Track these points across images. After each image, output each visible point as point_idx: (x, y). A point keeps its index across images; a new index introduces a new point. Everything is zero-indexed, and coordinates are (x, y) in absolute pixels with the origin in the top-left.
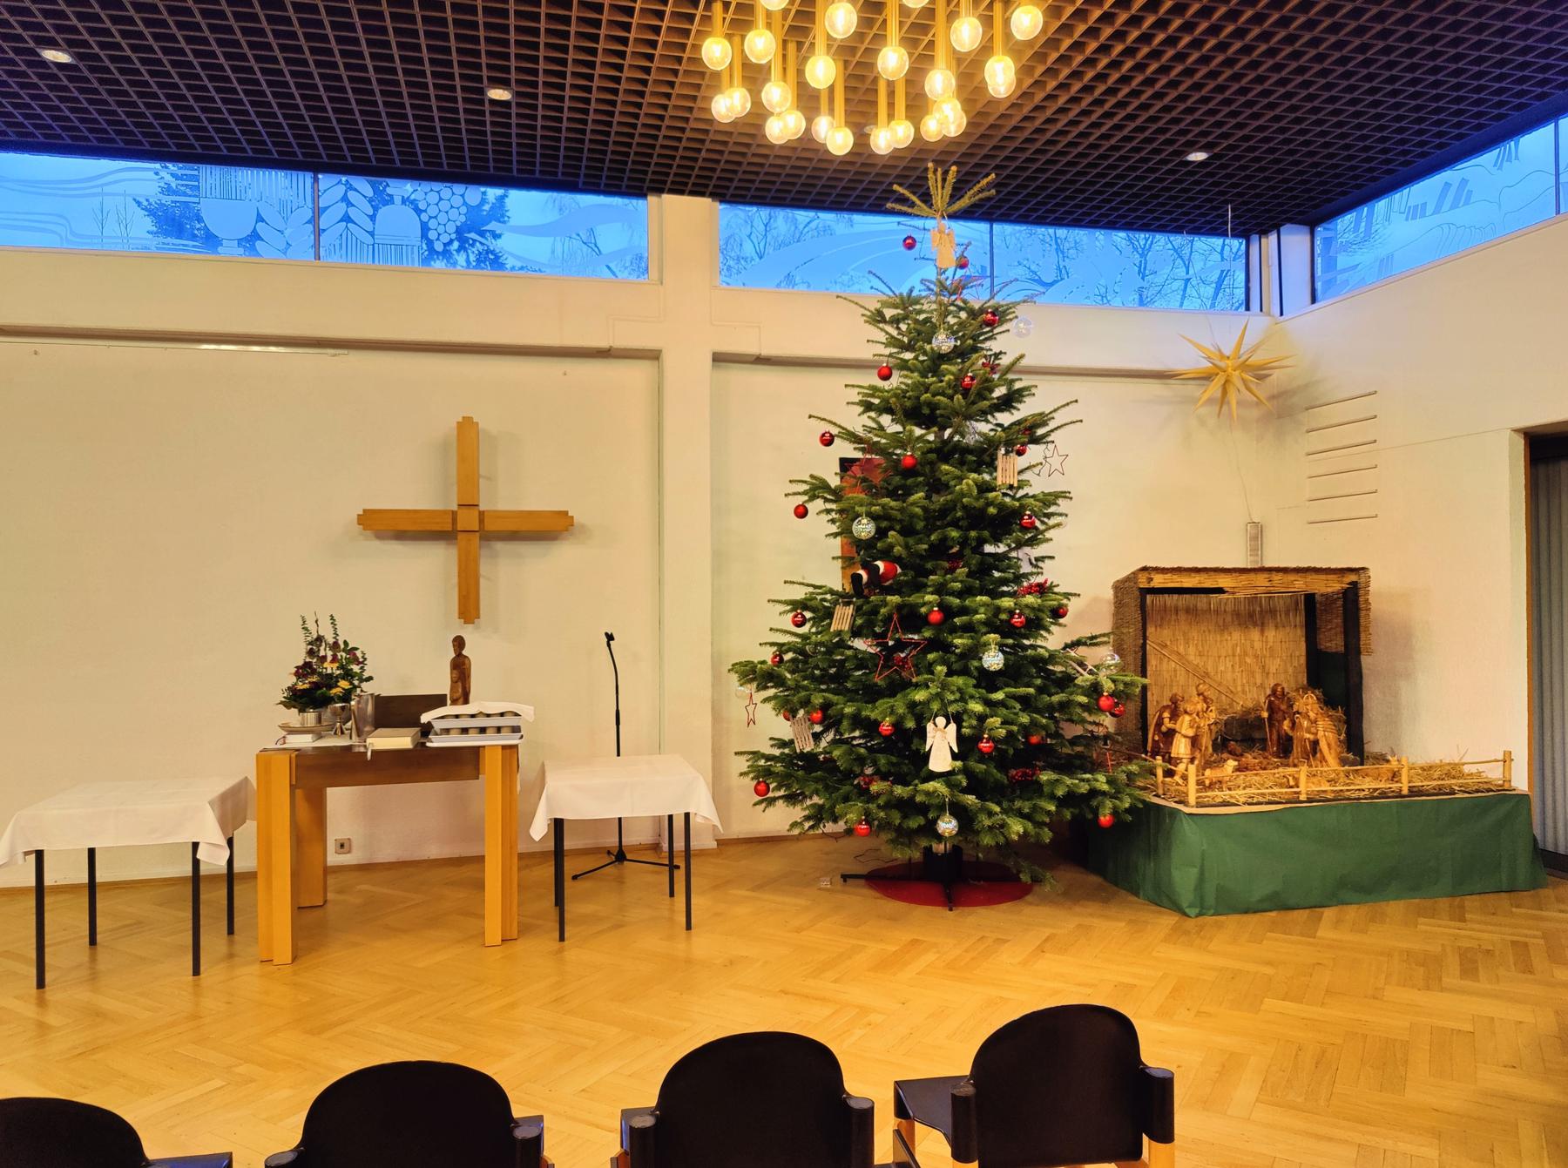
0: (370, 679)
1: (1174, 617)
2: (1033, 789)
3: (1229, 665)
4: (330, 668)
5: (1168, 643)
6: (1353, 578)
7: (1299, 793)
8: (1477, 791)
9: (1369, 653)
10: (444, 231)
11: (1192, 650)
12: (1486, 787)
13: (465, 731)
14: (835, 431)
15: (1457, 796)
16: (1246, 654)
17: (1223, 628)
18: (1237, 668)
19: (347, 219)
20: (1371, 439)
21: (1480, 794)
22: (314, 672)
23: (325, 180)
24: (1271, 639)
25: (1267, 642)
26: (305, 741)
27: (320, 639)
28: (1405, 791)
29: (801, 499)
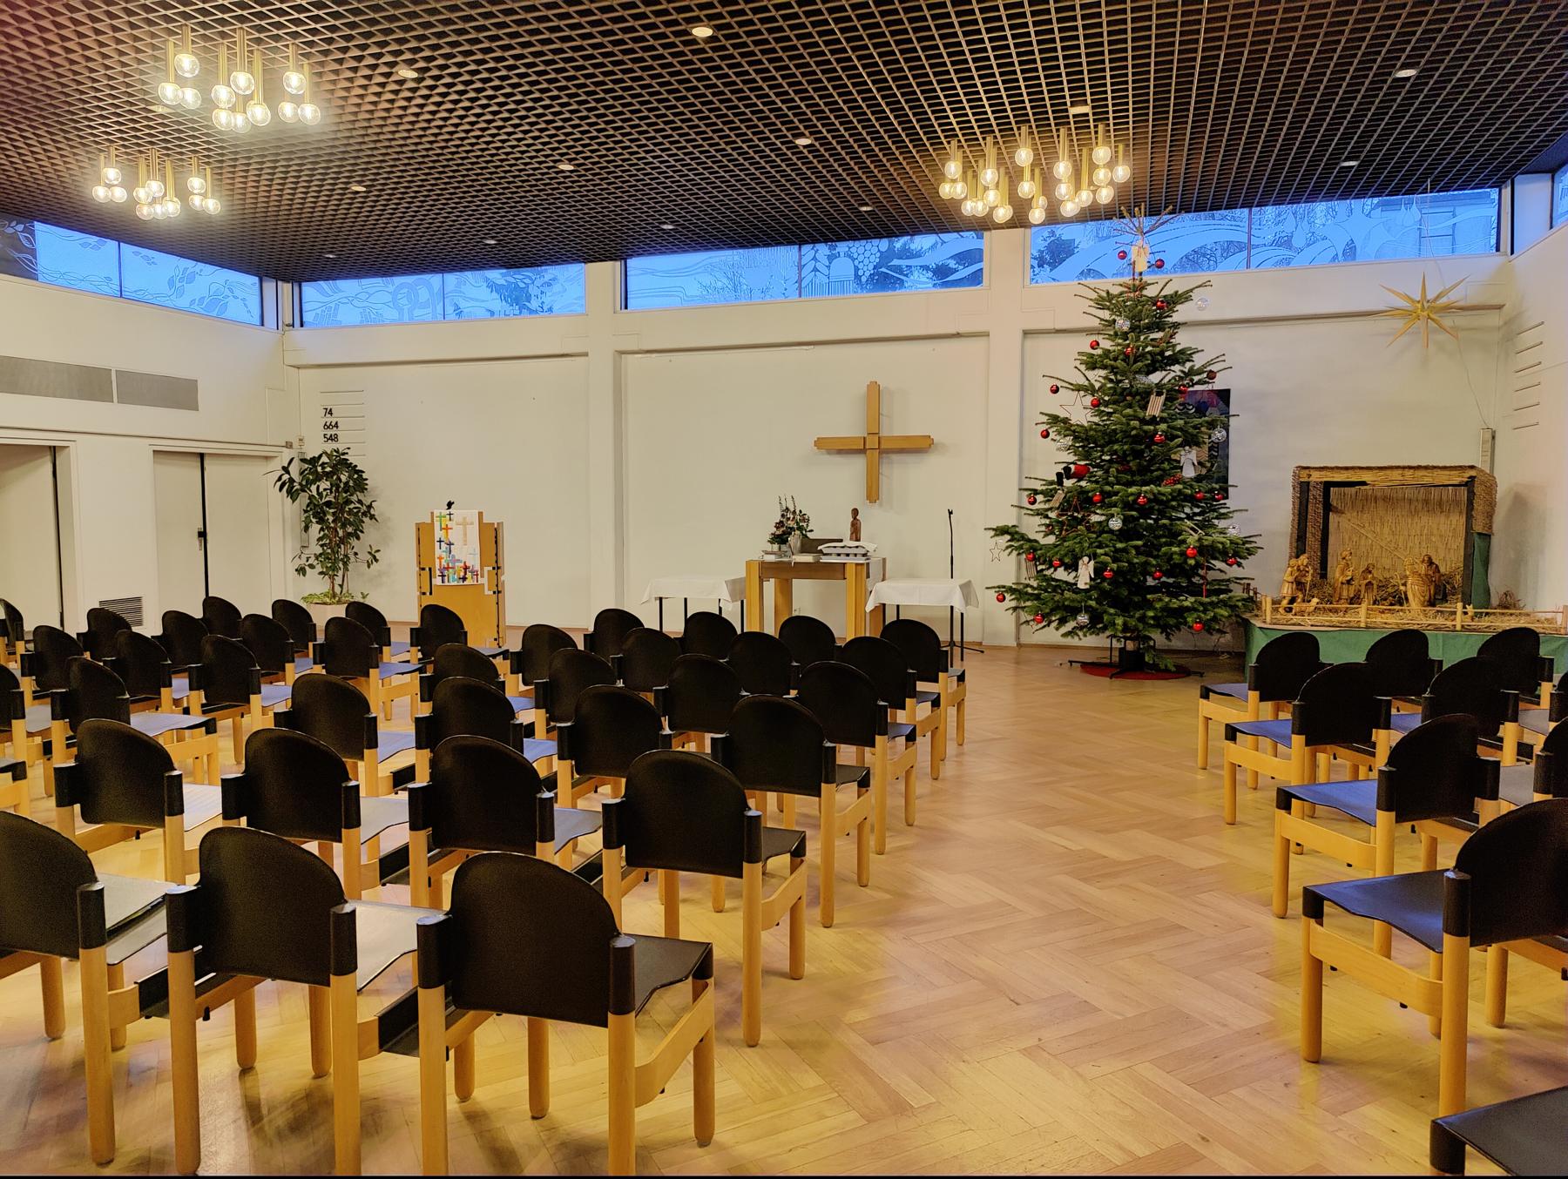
0: (811, 531)
2: (1149, 605)
3: (1417, 542)
4: (791, 524)
5: (1367, 525)
6: (1473, 473)
10: (867, 271)
11: (1386, 530)
13: (839, 555)
14: (1059, 384)
16: (1432, 534)
17: (1414, 513)
19: (815, 270)
20: (1537, 361)
22: (783, 526)
23: (806, 248)
24: (1454, 522)
26: (772, 558)
27: (787, 509)
29: (1045, 427)
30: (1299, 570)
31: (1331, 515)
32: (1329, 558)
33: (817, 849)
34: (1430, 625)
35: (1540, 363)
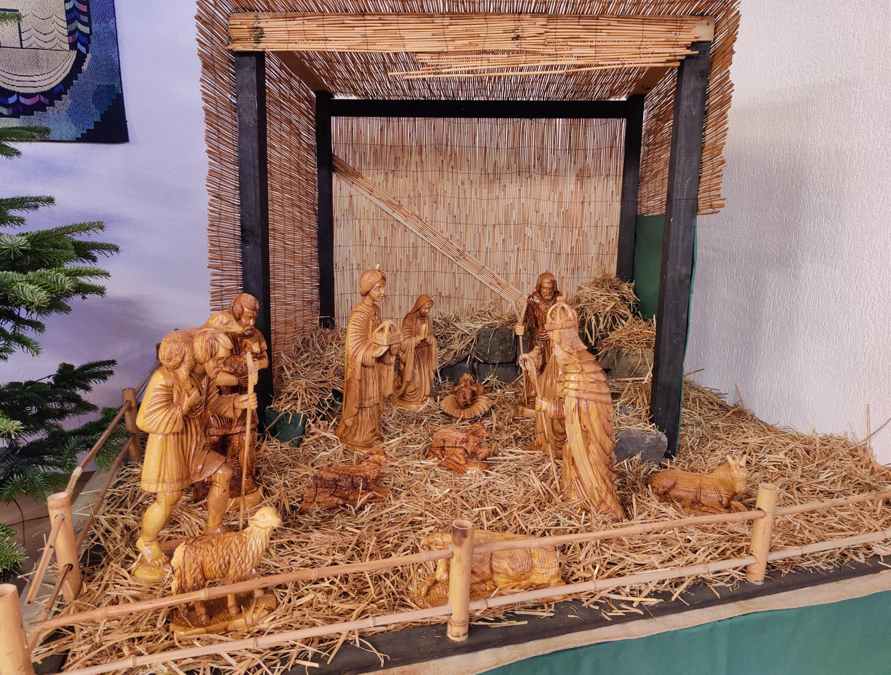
1: (415, 158)
3: (499, 239)
5: (405, 201)
9: (714, 209)
11: (442, 214)
16: (526, 222)
18: (511, 244)
25: (560, 202)
28: (757, 576)
31: (340, 186)
32: (337, 275)
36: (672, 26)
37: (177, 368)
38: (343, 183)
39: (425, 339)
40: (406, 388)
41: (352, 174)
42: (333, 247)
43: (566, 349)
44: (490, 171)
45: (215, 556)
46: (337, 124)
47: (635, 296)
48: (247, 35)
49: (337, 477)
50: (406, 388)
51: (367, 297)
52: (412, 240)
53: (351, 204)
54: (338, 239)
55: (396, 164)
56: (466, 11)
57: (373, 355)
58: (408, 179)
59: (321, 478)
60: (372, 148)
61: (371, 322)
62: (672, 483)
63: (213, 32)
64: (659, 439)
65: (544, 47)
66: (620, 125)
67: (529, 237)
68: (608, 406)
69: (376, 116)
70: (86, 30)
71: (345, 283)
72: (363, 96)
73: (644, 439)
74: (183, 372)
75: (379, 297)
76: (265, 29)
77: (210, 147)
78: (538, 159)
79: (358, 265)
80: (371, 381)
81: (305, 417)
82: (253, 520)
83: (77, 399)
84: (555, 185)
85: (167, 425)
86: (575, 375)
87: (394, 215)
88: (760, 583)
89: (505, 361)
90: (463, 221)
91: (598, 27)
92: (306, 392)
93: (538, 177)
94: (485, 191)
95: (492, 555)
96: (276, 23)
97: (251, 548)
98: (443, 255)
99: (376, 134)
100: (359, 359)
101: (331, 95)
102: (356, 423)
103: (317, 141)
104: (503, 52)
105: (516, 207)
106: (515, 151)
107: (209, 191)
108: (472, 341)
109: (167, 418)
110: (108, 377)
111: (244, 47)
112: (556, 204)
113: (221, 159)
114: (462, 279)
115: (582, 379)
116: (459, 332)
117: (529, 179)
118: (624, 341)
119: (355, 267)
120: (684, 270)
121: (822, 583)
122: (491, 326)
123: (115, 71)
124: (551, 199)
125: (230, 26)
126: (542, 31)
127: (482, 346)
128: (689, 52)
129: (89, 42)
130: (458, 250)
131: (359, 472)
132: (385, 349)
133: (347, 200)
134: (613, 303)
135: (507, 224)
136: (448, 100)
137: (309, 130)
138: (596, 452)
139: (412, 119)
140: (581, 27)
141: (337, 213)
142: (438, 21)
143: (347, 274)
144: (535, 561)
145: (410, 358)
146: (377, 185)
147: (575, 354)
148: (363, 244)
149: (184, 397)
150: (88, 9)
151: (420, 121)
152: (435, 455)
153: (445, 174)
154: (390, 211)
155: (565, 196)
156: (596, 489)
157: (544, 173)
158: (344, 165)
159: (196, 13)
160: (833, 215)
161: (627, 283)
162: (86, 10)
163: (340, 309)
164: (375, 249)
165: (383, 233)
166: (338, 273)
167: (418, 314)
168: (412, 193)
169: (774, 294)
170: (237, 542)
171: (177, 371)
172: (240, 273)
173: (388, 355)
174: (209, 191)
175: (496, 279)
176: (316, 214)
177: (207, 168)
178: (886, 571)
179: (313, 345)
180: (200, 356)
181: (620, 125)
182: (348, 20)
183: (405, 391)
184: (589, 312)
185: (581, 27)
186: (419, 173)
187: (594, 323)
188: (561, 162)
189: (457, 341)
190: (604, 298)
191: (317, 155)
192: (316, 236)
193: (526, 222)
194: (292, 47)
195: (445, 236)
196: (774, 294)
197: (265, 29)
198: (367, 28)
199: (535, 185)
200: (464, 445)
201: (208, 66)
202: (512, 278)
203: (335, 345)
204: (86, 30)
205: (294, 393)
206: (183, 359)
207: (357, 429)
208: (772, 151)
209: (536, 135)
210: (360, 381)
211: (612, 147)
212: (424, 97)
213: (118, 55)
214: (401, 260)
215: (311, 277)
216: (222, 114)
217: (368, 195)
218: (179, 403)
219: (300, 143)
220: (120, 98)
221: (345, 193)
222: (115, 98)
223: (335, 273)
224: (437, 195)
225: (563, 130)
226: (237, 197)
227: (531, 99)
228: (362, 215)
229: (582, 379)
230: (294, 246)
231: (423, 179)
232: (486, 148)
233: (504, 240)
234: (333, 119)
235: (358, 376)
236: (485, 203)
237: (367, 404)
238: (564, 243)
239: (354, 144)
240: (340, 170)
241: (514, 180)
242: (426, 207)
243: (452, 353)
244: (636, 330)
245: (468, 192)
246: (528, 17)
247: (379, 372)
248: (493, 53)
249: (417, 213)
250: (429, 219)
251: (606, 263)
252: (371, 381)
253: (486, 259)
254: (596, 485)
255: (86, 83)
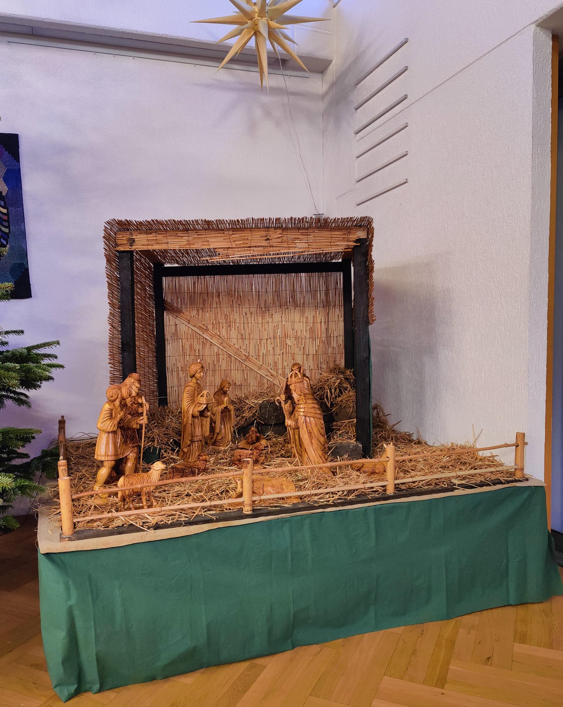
1: (215, 299)
5: (210, 327)
7: (242, 503)
8: (482, 485)
11: (234, 334)
12: (493, 477)
15: (456, 493)
16: (286, 336)
18: (278, 351)
21: (485, 489)
28: (390, 491)
30: (123, 405)
31: (169, 319)
32: (168, 375)
33: (239, 278)
34: (350, 492)
35: (405, 97)
36: (346, 232)
37: (114, 401)
38: (171, 317)
39: (227, 407)
40: (217, 437)
41: (176, 311)
42: (165, 357)
43: (298, 393)
44: (262, 306)
45: (138, 481)
46: (166, 281)
47: (354, 377)
48: (126, 242)
49: (184, 467)
50: (217, 437)
51: (194, 378)
52: (216, 351)
53: (176, 330)
54: (168, 352)
55: (204, 305)
56: (240, 227)
57: (198, 410)
58: (211, 313)
59: (176, 468)
60: (189, 294)
61: (196, 392)
62: (362, 465)
63: (110, 243)
64: (357, 446)
65: (281, 244)
66: (340, 276)
67: (289, 346)
68: (321, 420)
69: (191, 276)
70: (6, 230)
71: (174, 380)
72: (182, 264)
73: (349, 446)
74: (117, 403)
75: (200, 377)
76: (135, 239)
77: (110, 301)
78: (292, 297)
79: (182, 368)
80: (197, 426)
81: (160, 449)
82: (153, 466)
83: (16, 452)
84: (303, 312)
85: (111, 426)
86: (303, 405)
87: (204, 335)
88: (392, 494)
89: (278, 423)
90: (247, 337)
91: (308, 233)
92: (159, 437)
93: (292, 309)
94: (260, 318)
95: (263, 485)
96: (141, 236)
97: (152, 479)
98: (236, 359)
99: (191, 286)
100: (191, 412)
101: (163, 264)
102: (189, 451)
103: (154, 292)
104: (262, 246)
105: (280, 327)
106: (277, 293)
107: (109, 323)
108: (257, 411)
109: (111, 424)
110: (32, 441)
111: (124, 248)
112: (304, 324)
113: (114, 307)
114: (248, 374)
115: (306, 406)
116: (248, 406)
117: (287, 310)
118: (344, 400)
119: (180, 369)
120: (365, 355)
121: (425, 495)
122: (267, 401)
123: (24, 254)
124: (301, 321)
125: (116, 238)
126: (280, 236)
127: (264, 414)
128: (355, 244)
129: (8, 237)
130: (245, 355)
131: (195, 465)
132: (205, 406)
133: (173, 328)
134: (339, 381)
135: (275, 337)
136: (234, 265)
137: (150, 286)
138: (316, 443)
139: (212, 276)
140: (300, 233)
141: (168, 336)
142: (226, 232)
143: (175, 374)
144: (284, 487)
145: (218, 418)
146: (192, 317)
147: (303, 395)
148: (184, 355)
149: (117, 414)
150: (8, 218)
151: (217, 277)
152: (236, 464)
153: (235, 308)
154: (201, 333)
155: (309, 319)
156: (317, 462)
157: (296, 305)
158: (171, 306)
159: (103, 235)
160: (448, 323)
161: (349, 370)
162: (7, 219)
163: (171, 397)
164: (192, 357)
165: (197, 347)
166: (169, 374)
167: (222, 391)
168: (214, 321)
169: (429, 370)
170: (146, 476)
171: (114, 403)
172: (121, 368)
173: (206, 411)
174: (109, 323)
175: (270, 372)
176: (154, 337)
177: (109, 311)
178: (457, 490)
179: (157, 416)
180: (125, 395)
181: (340, 276)
182: (180, 234)
183: (216, 439)
184: (326, 387)
185: (300, 233)
186: (219, 309)
187: (329, 394)
188: (306, 299)
189: (247, 411)
190: (334, 379)
191: (155, 300)
192: (154, 350)
193: (286, 336)
194: (150, 248)
195: (236, 347)
196: (429, 370)
197: (135, 239)
198: (189, 237)
199: (290, 313)
200: (251, 456)
201: (109, 261)
202: (280, 371)
203: (170, 416)
204: (6, 230)
205: (152, 437)
206: (118, 396)
207: (190, 454)
208: (420, 289)
209: (290, 284)
210: (191, 424)
211: (336, 289)
212: (220, 263)
213: (26, 245)
214: (209, 363)
215: (153, 375)
216: (114, 283)
217: (187, 324)
218: (116, 417)
219: (146, 294)
220: (27, 270)
221: (172, 323)
222: (23, 270)
223: (167, 374)
224: (230, 322)
225: (306, 280)
226: (120, 326)
227: (285, 262)
228: (183, 336)
229: (306, 406)
230: (144, 355)
231: (221, 313)
232: (259, 292)
233: (273, 348)
234: (164, 278)
235: (190, 422)
236: (260, 325)
237: (195, 439)
238: (311, 347)
239: (177, 292)
240: (169, 309)
241: (277, 311)
242: (224, 329)
243: (244, 419)
244: (351, 394)
245: (249, 319)
246: (272, 229)
247: (201, 422)
248: (256, 247)
249: (218, 333)
250: (226, 337)
251: (338, 359)
252: (197, 426)
253: (263, 361)
254: (317, 460)
255: (6, 263)
